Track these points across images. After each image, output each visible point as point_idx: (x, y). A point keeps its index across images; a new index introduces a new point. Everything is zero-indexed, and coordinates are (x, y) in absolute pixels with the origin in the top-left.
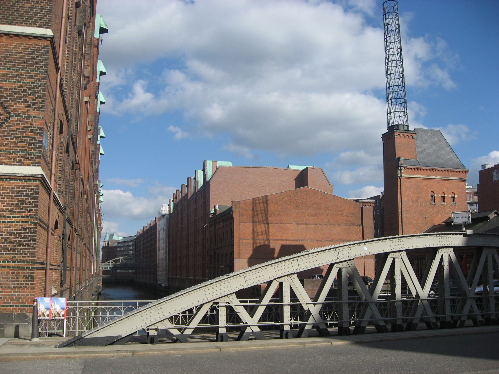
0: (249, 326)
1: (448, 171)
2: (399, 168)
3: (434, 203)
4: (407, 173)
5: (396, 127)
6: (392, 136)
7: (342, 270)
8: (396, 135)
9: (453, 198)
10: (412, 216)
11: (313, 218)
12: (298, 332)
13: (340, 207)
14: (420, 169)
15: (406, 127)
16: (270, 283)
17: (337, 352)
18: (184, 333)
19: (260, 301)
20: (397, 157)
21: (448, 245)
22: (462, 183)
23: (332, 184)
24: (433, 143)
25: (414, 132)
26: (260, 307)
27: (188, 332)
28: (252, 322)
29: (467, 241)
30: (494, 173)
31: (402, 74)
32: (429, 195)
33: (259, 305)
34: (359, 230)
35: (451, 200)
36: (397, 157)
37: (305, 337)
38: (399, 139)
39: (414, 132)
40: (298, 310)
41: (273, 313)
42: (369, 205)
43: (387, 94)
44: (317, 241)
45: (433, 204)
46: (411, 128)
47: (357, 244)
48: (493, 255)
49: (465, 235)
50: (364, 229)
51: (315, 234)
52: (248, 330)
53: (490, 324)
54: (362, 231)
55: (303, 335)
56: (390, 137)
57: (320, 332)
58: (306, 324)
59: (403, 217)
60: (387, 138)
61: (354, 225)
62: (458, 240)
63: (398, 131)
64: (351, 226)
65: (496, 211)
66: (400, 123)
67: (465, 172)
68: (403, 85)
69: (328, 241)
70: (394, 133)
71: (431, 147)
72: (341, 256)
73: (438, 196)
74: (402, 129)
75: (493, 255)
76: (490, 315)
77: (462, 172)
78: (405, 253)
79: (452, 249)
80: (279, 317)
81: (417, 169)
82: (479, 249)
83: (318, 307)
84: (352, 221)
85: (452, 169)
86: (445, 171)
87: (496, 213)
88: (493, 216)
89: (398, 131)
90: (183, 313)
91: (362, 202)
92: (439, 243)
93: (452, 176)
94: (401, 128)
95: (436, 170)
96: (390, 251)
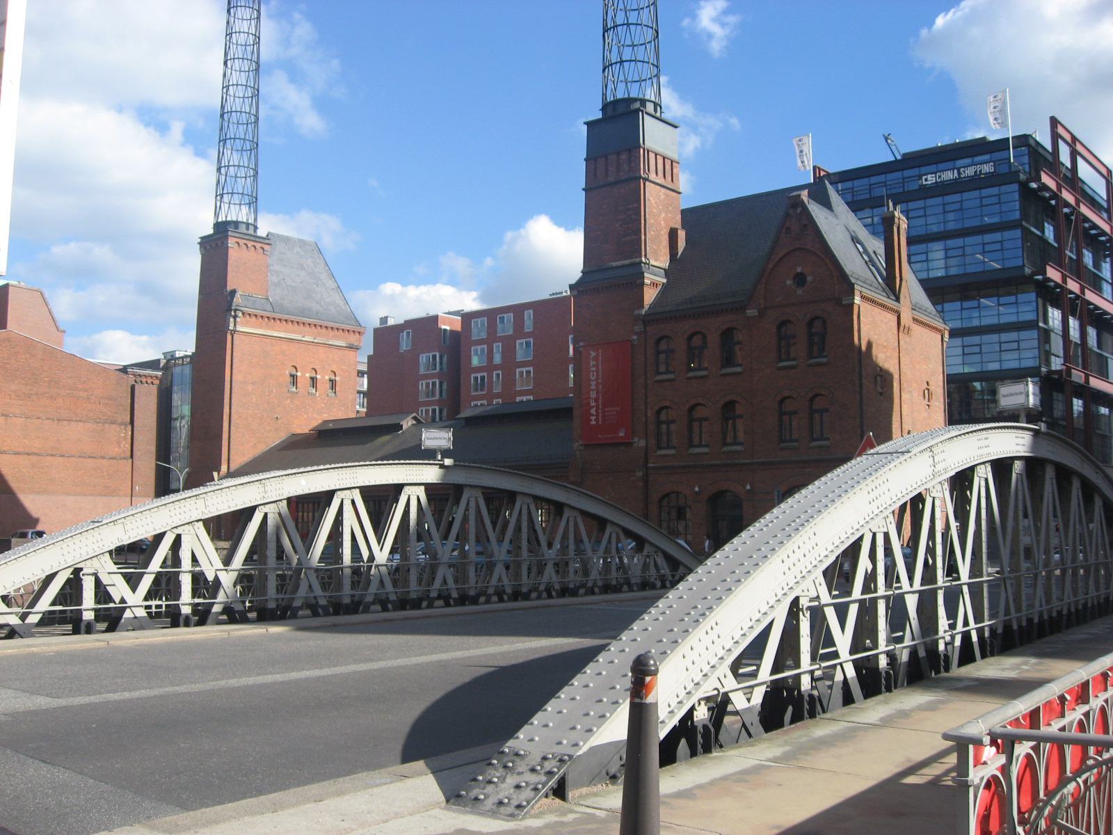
0: (130, 607)
1: (326, 327)
2: (233, 313)
3: (294, 389)
4: (246, 325)
5: (233, 225)
6: (222, 243)
7: (269, 516)
8: (231, 242)
9: (333, 383)
10: (250, 412)
11: (21, 402)
12: (202, 616)
13: (85, 382)
14: (274, 319)
15: (251, 228)
16: (159, 538)
17: (277, 638)
18: (26, 622)
19: (146, 566)
20: (229, 288)
21: (418, 482)
22: (351, 353)
23: (62, 328)
24: (302, 267)
25: (267, 241)
26: (145, 576)
27: (33, 619)
28: (135, 601)
29: (444, 476)
30: (403, 336)
31: (256, 116)
32: (287, 372)
33: (145, 573)
34: (123, 435)
35: (328, 385)
36: (229, 288)
37: (210, 625)
38: (236, 253)
39: (267, 241)
40: (202, 583)
41: (166, 585)
42: (149, 381)
43: (219, 152)
44: (28, 454)
45: (293, 392)
46: (262, 232)
47: (291, 474)
48: (476, 498)
49: (442, 466)
50: (135, 432)
51: (25, 438)
52: (128, 614)
53: (408, 607)
54: (129, 437)
55: (209, 621)
56: (217, 244)
57: (233, 615)
58: (214, 603)
59: (232, 414)
60: (211, 246)
61: (113, 423)
62: (431, 474)
63: (237, 235)
64: (106, 425)
65: (414, 414)
66: (240, 219)
67: (359, 333)
68: (255, 140)
69: (52, 455)
70: (227, 237)
71: (299, 276)
72: (269, 494)
73: (304, 376)
74: (248, 232)
75: (476, 498)
76: (408, 592)
77: (354, 332)
78: (358, 490)
79: (422, 488)
80: (175, 592)
81: (268, 318)
82: (458, 489)
83: (234, 575)
84: (110, 414)
85: (335, 325)
86: (321, 326)
87: (415, 418)
88: (410, 424)
89: (237, 235)
90: (15, 591)
91: (135, 376)
92: (406, 477)
93: (334, 337)
94: (243, 229)
95: (304, 324)
96: (338, 487)
